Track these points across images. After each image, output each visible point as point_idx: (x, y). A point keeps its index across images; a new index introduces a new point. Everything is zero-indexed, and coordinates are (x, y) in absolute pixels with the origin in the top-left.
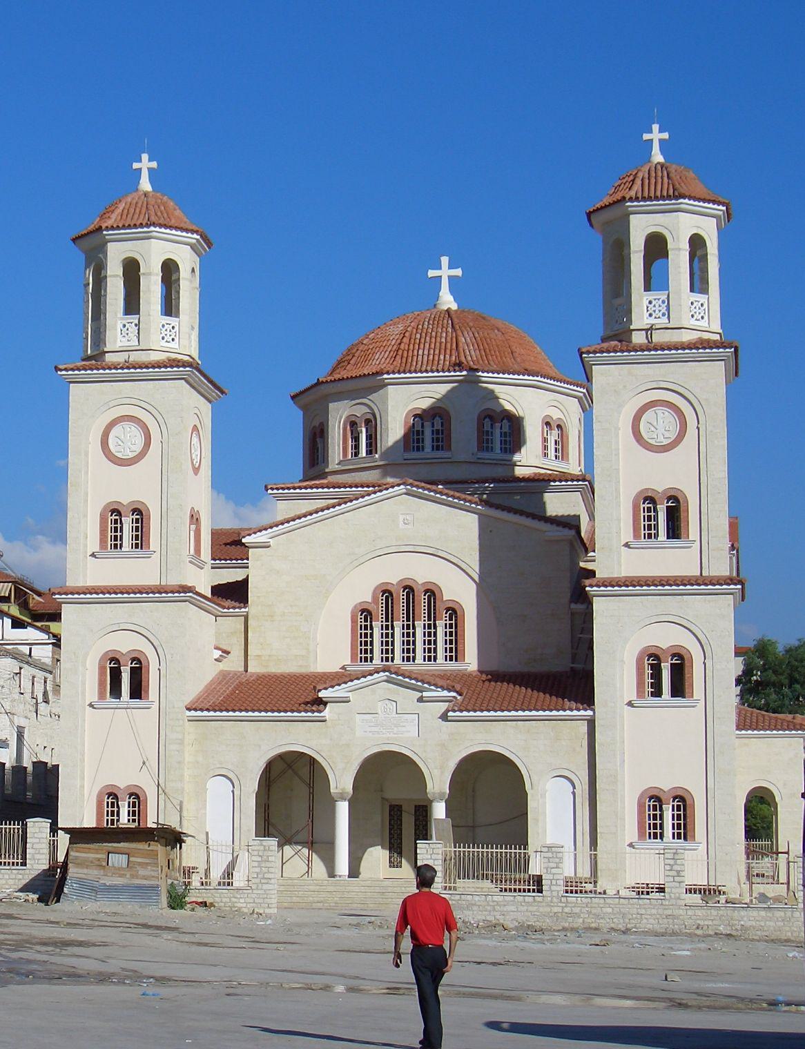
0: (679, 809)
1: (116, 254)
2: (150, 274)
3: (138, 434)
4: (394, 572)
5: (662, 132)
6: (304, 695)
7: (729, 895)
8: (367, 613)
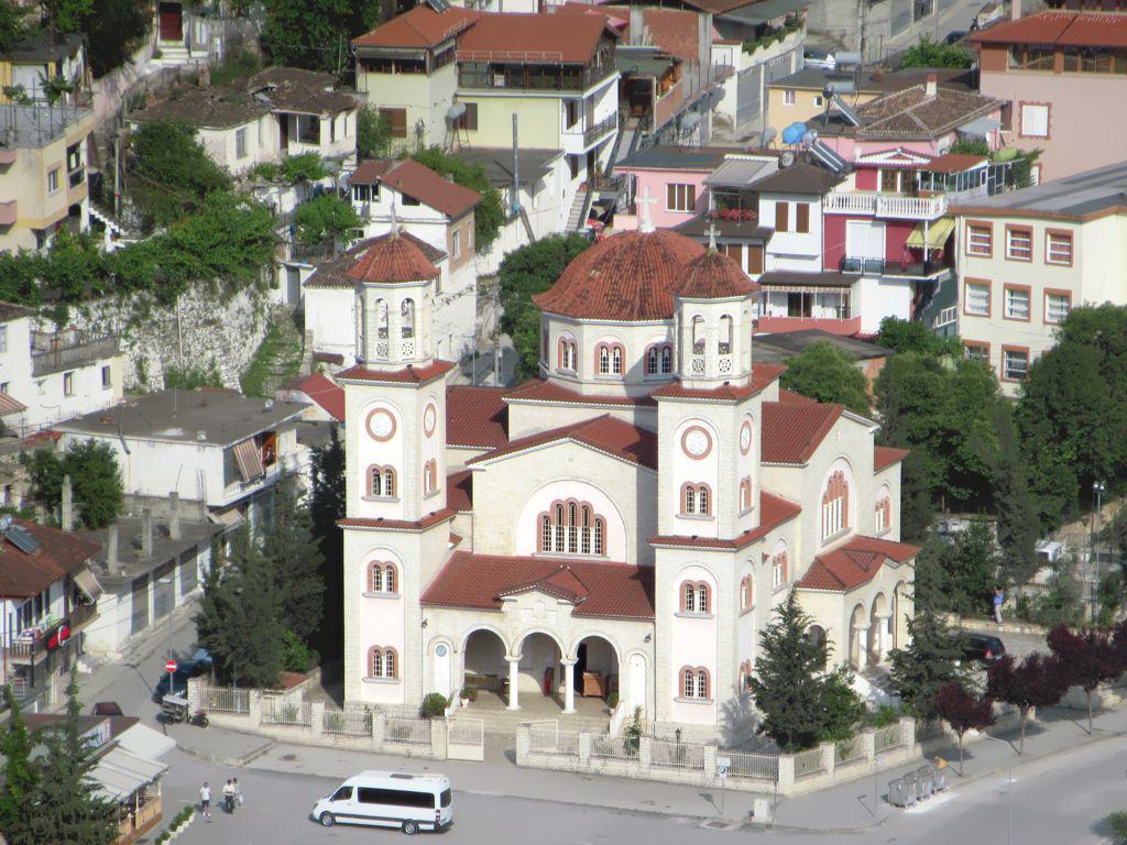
2: (394, 313)
4: (581, 494)
5: (319, 137)
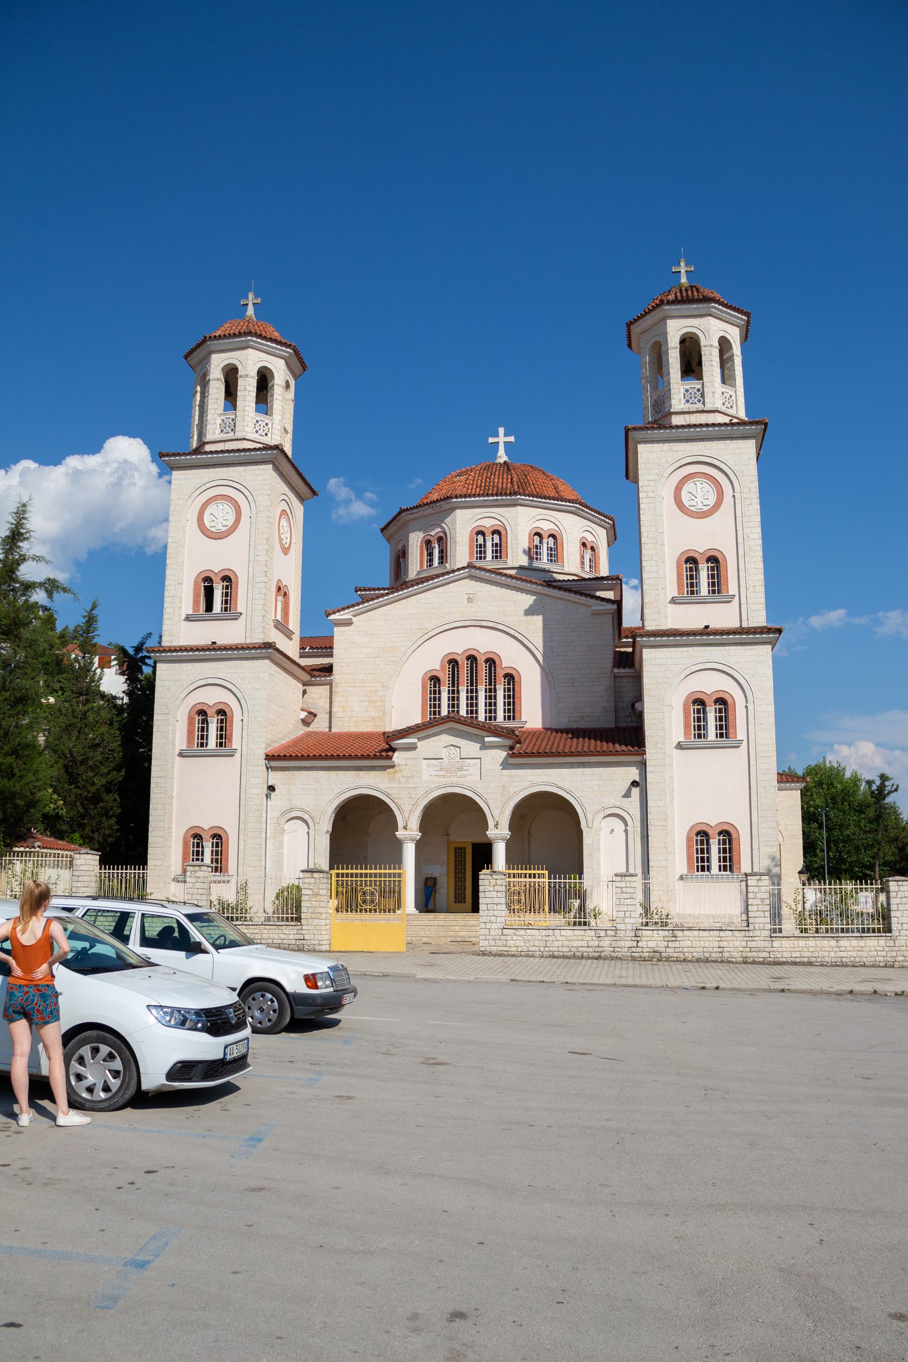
0: (724, 843)
1: (217, 363)
3: (230, 510)
4: (459, 644)
6: (381, 750)
7: (563, 921)
8: (435, 680)
